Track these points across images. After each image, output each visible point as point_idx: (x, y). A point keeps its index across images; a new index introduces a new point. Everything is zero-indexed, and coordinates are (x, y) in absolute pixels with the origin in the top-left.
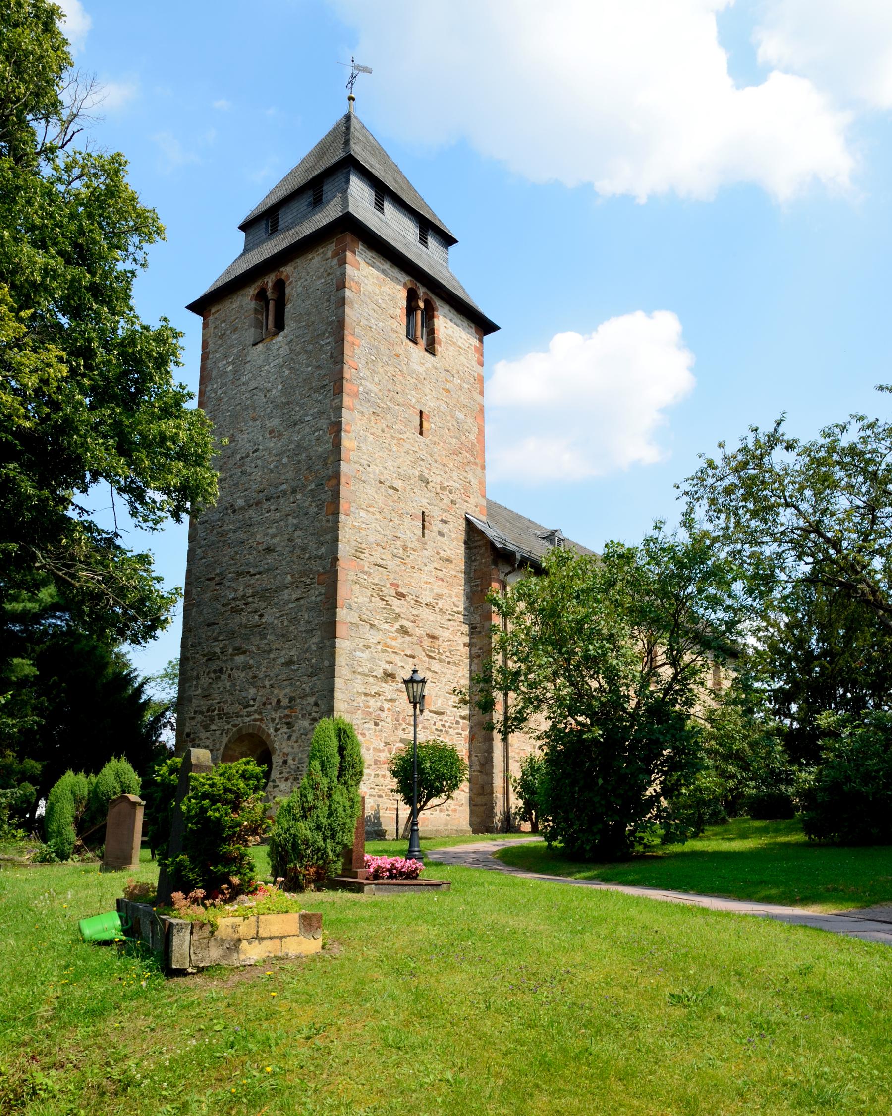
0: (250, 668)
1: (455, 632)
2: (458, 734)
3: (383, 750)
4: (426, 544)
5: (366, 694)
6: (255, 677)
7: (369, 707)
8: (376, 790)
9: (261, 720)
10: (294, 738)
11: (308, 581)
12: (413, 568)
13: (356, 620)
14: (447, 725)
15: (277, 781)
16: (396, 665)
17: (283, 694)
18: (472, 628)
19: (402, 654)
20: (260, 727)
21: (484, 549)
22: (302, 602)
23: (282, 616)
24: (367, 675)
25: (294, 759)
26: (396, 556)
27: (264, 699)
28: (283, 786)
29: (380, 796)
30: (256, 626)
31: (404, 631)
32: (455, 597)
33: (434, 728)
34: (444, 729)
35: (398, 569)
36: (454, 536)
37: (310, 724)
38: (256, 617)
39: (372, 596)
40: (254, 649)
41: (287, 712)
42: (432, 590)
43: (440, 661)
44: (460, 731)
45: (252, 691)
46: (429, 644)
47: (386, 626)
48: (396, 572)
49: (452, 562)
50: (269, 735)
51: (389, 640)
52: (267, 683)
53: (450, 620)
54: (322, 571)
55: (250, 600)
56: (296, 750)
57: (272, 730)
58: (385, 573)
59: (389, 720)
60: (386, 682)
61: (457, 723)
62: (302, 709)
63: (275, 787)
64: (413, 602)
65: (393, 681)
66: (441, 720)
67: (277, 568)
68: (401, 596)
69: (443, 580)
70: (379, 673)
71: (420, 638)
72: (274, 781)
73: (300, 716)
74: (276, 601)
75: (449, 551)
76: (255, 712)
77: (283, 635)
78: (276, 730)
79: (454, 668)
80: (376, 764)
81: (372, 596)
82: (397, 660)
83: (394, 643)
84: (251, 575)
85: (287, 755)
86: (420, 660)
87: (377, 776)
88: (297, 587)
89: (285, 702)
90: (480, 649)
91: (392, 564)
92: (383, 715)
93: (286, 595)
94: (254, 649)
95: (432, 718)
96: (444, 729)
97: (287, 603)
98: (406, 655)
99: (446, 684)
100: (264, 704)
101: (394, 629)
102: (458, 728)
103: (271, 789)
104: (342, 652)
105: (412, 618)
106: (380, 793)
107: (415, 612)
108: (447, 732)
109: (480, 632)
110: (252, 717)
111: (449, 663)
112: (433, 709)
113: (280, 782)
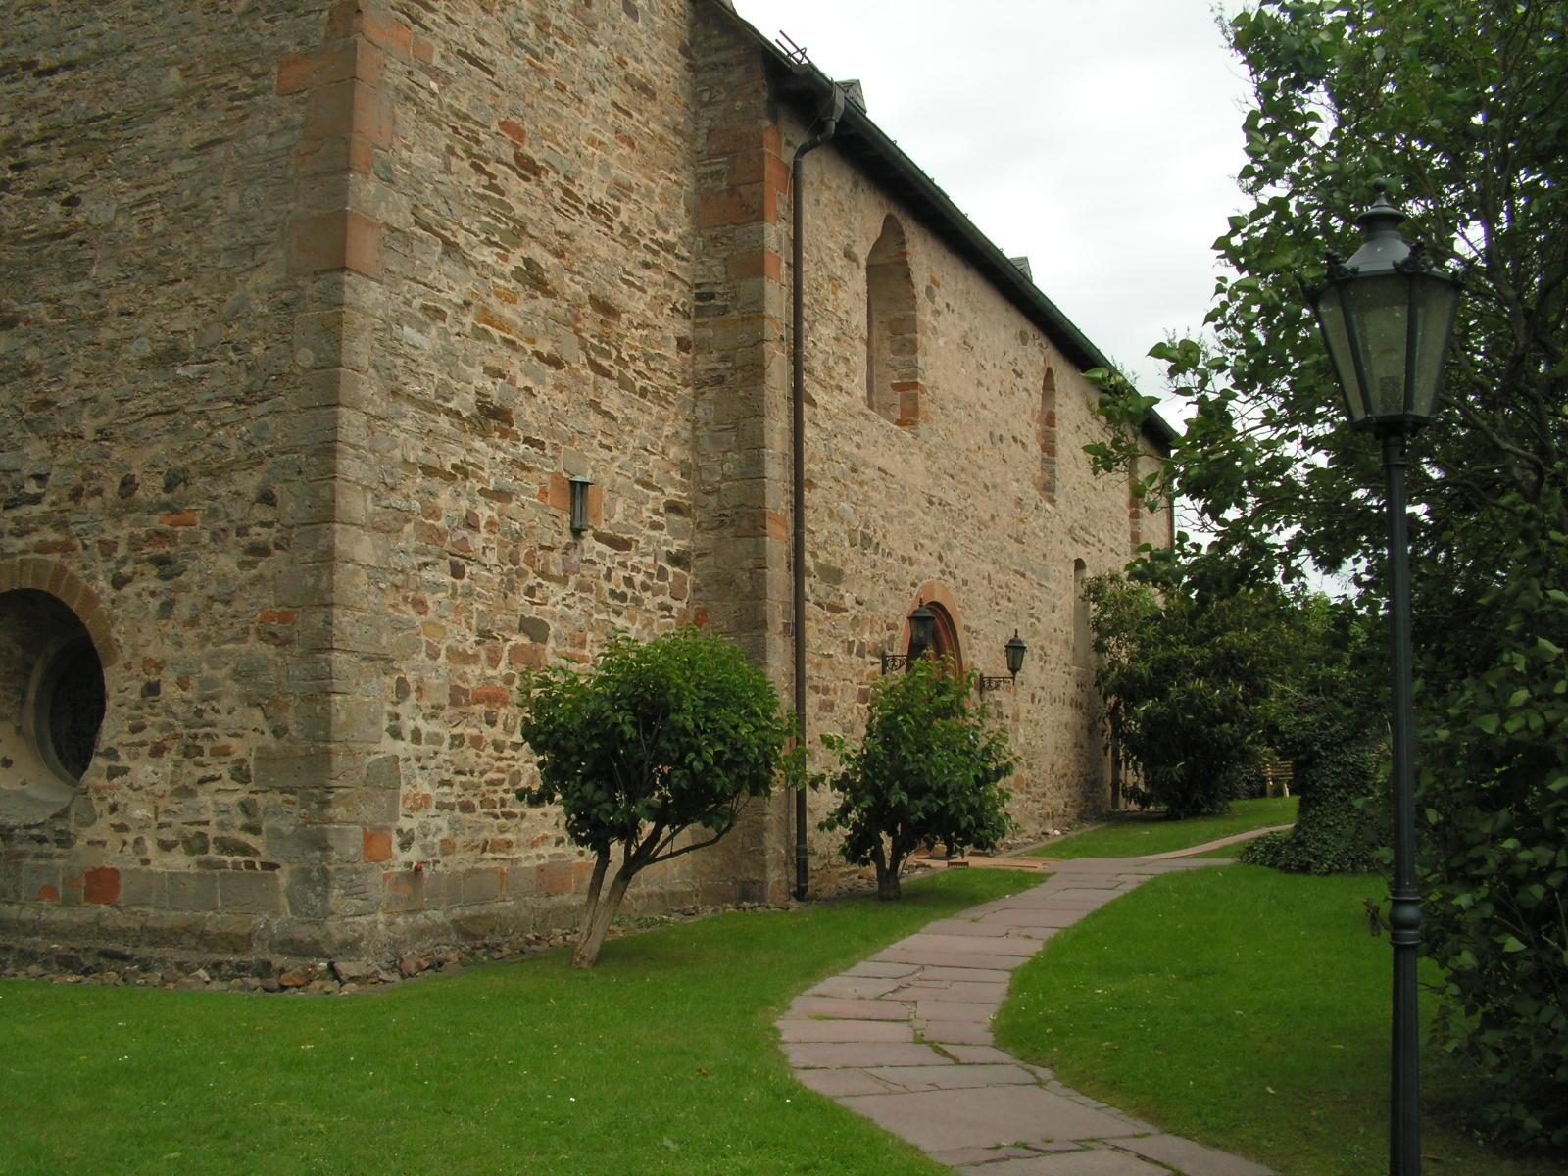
0: (29, 374)
1: (658, 302)
2: (663, 607)
3: (476, 657)
4: (593, 26)
5: (429, 471)
6: (47, 403)
7: (435, 514)
8: (457, 789)
9: (66, 548)
10: (183, 610)
11: (244, 86)
12: (562, 89)
13: (402, 219)
14: (639, 578)
15: (123, 754)
16: (512, 382)
17: (146, 458)
18: (699, 297)
19: (529, 348)
20: (61, 570)
21: (740, 71)
22: (219, 153)
23: (147, 200)
24: (432, 408)
25: (183, 684)
26: (516, 41)
27: (76, 477)
28: (144, 770)
29: (467, 807)
30: (53, 237)
31: (532, 277)
32: (659, 201)
33: (606, 586)
34: (629, 592)
35: (522, 81)
36: (659, 23)
37: (242, 565)
38: (55, 208)
39: (450, 150)
40: (42, 311)
41: (158, 522)
42: (605, 167)
43: (625, 384)
44: (668, 599)
45: (36, 450)
46: (598, 329)
47: (488, 255)
48: (514, 91)
49: (652, 96)
50: (91, 599)
51: (493, 300)
52: (88, 425)
53: (646, 265)
54: (292, 47)
55: (34, 152)
56: (192, 651)
57: (103, 583)
58: (488, 86)
59: (492, 558)
60: (485, 435)
61: (662, 574)
62: (213, 513)
63: (113, 773)
64: (558, 193)
65: (504, 435)
66: (623, 565)
67: (130, 49)
68: (528, 168)
69: (632, 145)
70: (465, 402)
71: (575, 305)
72: (111, 754)
73: (206, 537)
74: (124, 151)
75: (647, 63)
76: (45, 519)
77: (148, 267)
78: (119, 582)
79: (655, 409)
80: (454, 703)
81: (450, 150)
82: (515, 366)
83: (507, 312)
84: (39, 74)
85: (159, 667)
86: (574, 374)
87: (457, 741)
88: (202, 105)
89: (150, 489)
90: (724, 359)
91: (508, 64)
92: (477, 541)
93: (160, 133)
94: (42, 311)
95: (601, 555)
96: (629, 592)
97: (160, 162)
98: (537, 354)
99: (635, 457)
100: (76, 494)
101: (508, 268)
102: (661, 591)
103: (103, 782)
104: (360, 320)
105: (555, 241)
106: (468, 796)
107: (563, 226)
108: (638, 601)
109: (725, 309)
110: (35, 538)
111: (643, 392)
112: (603, 528)
113: (135, 757)
